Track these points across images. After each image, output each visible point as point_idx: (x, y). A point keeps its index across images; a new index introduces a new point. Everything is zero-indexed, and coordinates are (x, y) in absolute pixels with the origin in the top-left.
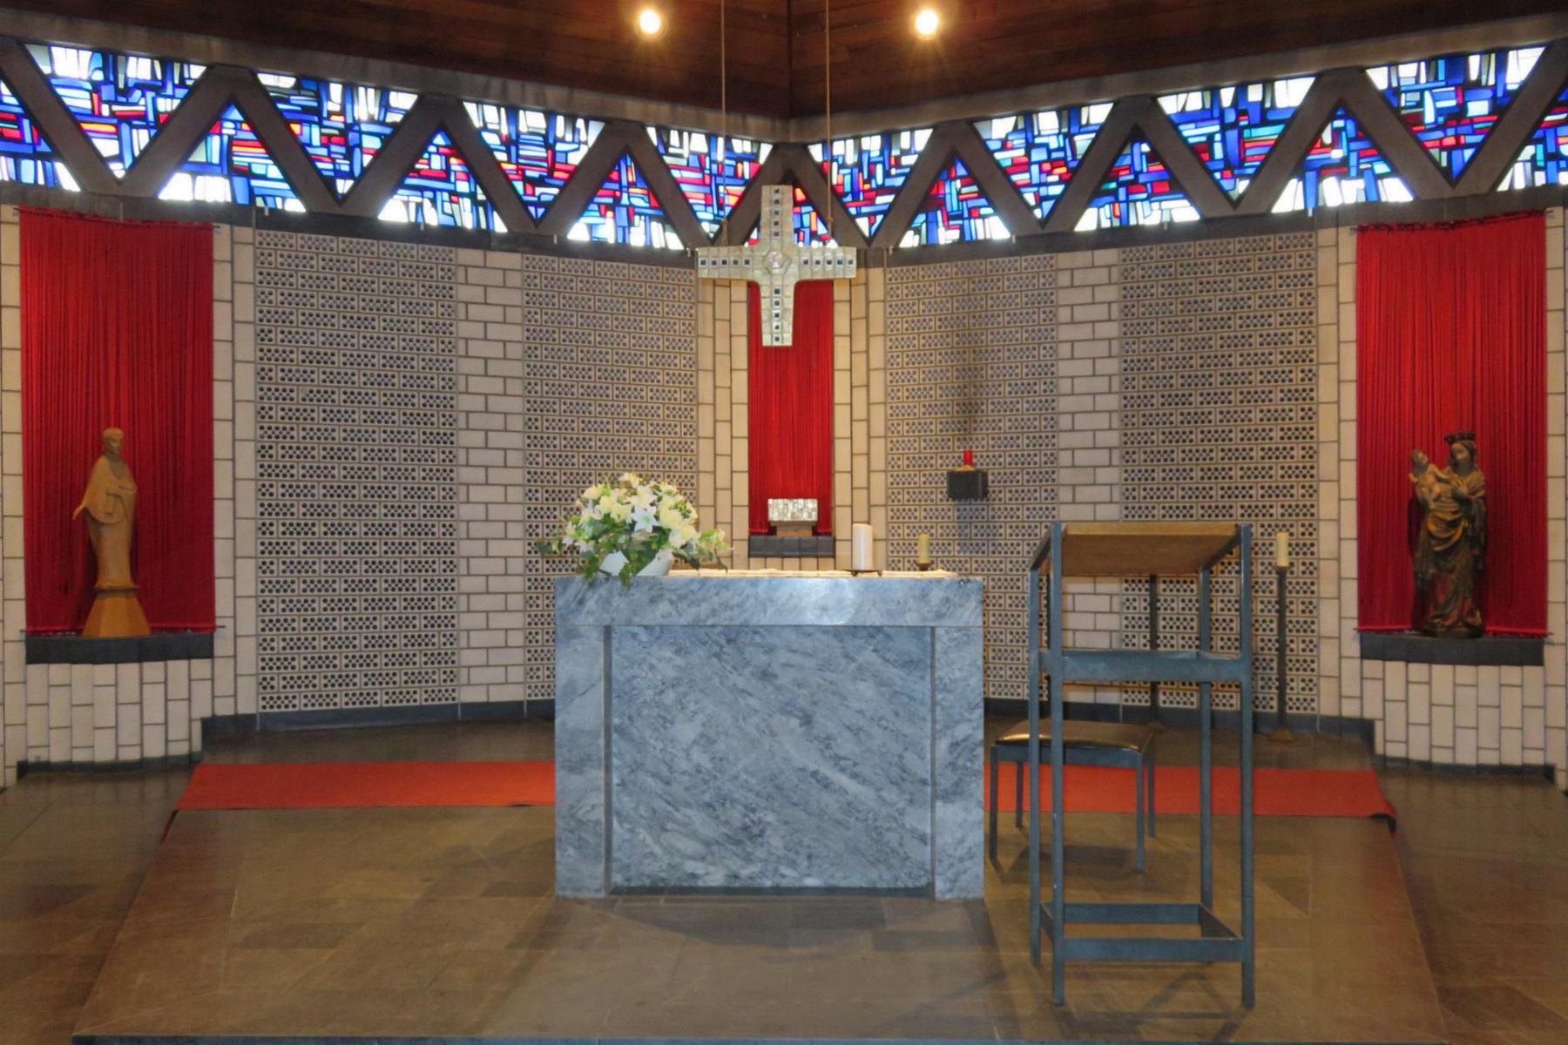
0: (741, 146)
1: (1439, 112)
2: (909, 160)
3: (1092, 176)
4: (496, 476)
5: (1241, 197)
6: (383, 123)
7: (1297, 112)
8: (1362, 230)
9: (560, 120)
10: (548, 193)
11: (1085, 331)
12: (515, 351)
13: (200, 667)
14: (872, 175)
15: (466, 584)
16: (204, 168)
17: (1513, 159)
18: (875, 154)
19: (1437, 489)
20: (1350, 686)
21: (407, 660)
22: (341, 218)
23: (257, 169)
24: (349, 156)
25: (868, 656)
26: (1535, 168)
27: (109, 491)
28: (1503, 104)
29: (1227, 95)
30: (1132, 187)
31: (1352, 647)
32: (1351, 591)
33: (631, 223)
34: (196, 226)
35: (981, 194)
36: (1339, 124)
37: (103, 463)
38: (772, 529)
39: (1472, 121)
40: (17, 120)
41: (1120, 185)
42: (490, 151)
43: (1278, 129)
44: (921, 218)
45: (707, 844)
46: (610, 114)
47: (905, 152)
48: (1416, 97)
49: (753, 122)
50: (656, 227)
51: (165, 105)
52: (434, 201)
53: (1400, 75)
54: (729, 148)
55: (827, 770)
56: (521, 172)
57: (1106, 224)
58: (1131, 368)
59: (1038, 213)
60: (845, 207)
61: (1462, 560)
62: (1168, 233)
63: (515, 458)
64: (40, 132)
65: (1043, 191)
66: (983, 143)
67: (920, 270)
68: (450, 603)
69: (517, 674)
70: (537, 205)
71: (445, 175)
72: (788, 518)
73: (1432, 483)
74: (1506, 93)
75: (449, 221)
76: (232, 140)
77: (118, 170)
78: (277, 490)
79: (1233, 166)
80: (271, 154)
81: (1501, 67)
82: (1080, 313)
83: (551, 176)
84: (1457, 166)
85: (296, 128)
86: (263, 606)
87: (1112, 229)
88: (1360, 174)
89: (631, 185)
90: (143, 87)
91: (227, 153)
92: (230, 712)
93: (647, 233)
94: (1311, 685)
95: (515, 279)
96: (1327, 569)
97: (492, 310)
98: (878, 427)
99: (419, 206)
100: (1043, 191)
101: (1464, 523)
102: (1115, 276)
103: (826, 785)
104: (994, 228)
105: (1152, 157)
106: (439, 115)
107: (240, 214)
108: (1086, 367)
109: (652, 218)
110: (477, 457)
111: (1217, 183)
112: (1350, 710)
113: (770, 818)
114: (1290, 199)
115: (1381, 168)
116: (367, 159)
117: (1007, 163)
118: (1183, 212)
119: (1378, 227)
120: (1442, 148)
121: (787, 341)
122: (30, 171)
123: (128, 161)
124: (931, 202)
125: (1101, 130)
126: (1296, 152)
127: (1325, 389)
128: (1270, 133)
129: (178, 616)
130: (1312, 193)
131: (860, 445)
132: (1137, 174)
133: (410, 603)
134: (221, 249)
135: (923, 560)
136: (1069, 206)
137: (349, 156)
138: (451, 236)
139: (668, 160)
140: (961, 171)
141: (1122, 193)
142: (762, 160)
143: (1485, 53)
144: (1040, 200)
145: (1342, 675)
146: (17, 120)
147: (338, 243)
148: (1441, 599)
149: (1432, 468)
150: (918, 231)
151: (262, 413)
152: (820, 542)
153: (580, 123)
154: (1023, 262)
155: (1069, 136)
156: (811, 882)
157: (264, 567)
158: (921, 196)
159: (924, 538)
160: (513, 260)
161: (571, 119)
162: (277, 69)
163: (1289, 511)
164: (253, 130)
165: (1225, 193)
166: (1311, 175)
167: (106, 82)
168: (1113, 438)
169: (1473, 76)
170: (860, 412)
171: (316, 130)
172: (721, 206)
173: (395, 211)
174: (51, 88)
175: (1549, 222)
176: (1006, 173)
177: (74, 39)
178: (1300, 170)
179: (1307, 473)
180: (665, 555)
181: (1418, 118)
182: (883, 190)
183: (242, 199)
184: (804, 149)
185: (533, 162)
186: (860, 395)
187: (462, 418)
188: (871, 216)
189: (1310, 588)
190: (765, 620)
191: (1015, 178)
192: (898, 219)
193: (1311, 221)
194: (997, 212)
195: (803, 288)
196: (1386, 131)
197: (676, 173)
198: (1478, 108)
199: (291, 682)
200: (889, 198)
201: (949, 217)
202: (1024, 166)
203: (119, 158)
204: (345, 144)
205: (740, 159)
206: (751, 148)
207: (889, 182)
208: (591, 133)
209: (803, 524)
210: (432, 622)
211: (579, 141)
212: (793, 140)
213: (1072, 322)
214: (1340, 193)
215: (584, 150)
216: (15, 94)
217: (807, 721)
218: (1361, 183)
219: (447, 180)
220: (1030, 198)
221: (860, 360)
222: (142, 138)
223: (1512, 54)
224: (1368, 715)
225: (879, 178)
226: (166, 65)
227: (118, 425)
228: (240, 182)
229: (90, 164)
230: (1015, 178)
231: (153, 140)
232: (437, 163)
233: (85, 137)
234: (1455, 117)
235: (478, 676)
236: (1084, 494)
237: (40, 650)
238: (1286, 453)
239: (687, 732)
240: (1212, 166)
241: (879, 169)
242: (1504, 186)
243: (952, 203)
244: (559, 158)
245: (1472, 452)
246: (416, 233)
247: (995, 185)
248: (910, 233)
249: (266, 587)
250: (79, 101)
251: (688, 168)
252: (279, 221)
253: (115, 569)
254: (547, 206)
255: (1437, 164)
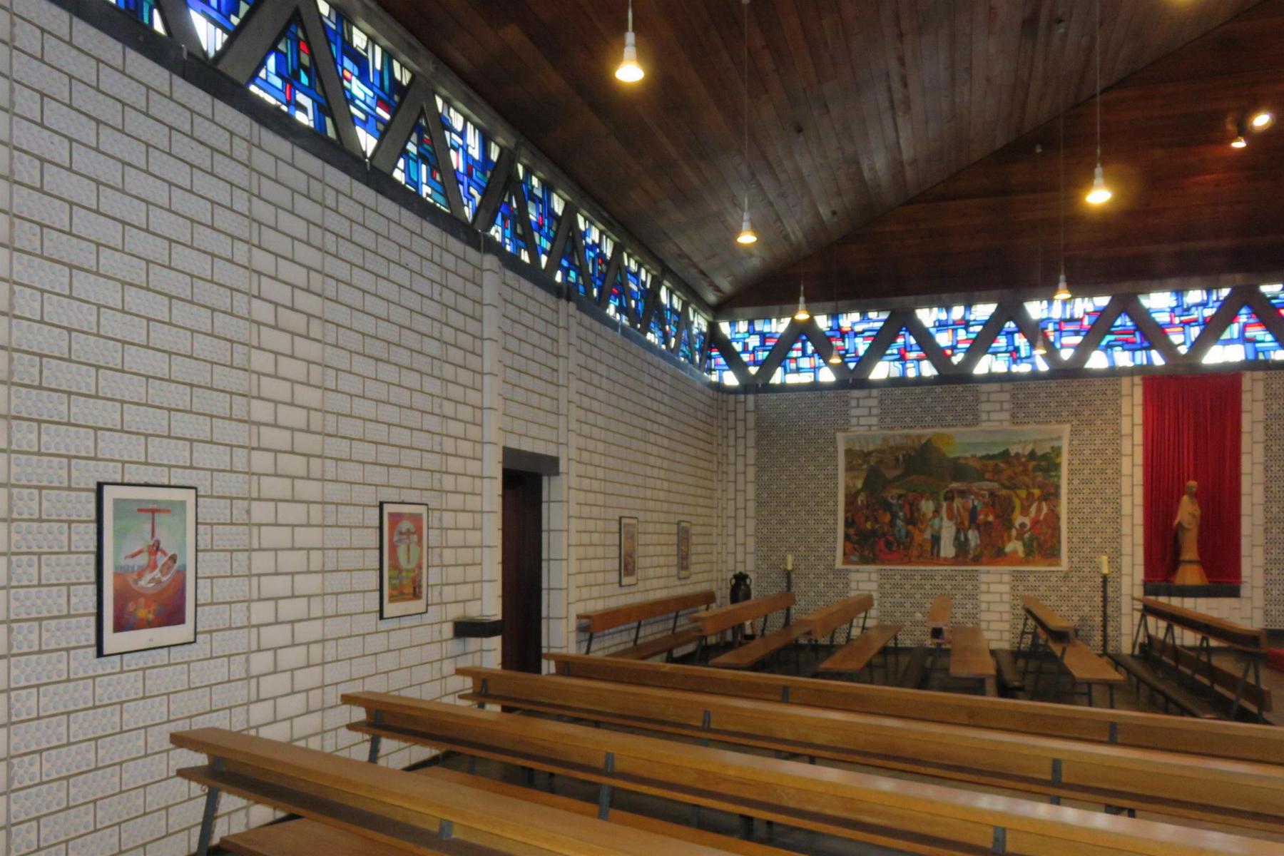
16: (1230, 341)
23: (1259, 338)
27: (1187, 512)
37: (1185, 498)
64: (1144, 336)
76: (1246, 325)
90: (1197, 305)
104: (730, 379)
122: (1141, 358)
123: (1188, 344)
129: (1223, 576)
183: (1251, 357)
203: (1184, 343)
222: (1195, 332)
226: (1209, 292)
227: (1195, 479)
228: (1249, 346)
229: (1169, 350)
231: (1202, 332)
237: (551, 465)
250: (1162, 318)
253: (1190, 551)
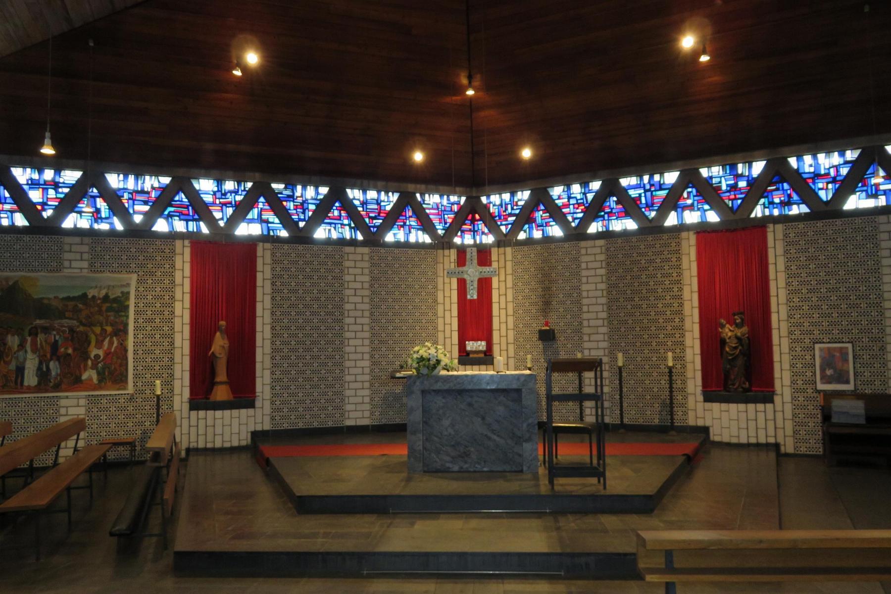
0: (454, 198)
1: (728, 185)
2: (521, 203)
3: (594, 210)
4: (359, 335)
5: (653, 218)
6: (316, 199)
7: (674, 186)
8: (698, 233)
9: (383, 193)
10: (378, 222)
11: (592, 272)
12: (366, 285)
13: (251, 411)
14: (506, 209)
15: (348, 378)
16: (252, 221)
17: (756, 204)
18: (508, 200)
19: (730, 334)
20: (700, 413)
21: (325, 408)
22: (301, 237)
23: (270, 220)
24: (304, 213)
25: (502, 398)
26: (765, 207)
27: (220, 344)
28: (752, 183)
29: (646, 178)
30: (610, 214)
31: (701, 398)
32: (699, 375)
33: (410, 232)
34: (251, 243)
35: (550, 217)
36: (690, 190)
38: (468, 354)
39: (740, 189)
40: (187, 207)
41: (606, 213)
42: (356, 207)
43: (666, 191)
44: (526, 226)
45: (453, 458)
46: (402, 190)
47: (519, 200)
48: (718, 180)
49: (458, 189)
50: (420, 233)
51: (239, 198)
52: (335, 228)
53: (713, 172)
54: (448, 199)
55: (490, 434)
56: (368, 214)
57: (600, 230)
58: (611, 287)
59: (573, 225)
60: (496, 222)
61: (740, 362)
62: (625, 234)
63: (366, 328)
64: (195, 211)
65: (575, 216)
66: (551, 197)
67: (526, 248)
68: (342, 386)
69: (367, 414)
70: (374, 227)
71: (339, 218)
72: (474, 349)
73: (728, 331)
74: (753, 179)
75: (341, 236)
77: (222, 224)
78: (278, 343)
79: (649, 206)
80: (276, 214)
81: (750, 167)
82: (590, 265)
83: (379, 215)
84: (735, 207)
85: (285, 203)
86: (272, 388)
87: (603, 232)
88: (699, 209)
89: (410, 217)
90: (231, 192)
91: (260, 215)
92: (260, 429)
93: (417, 235)
94: (685, 413)
95: (366, 258)
96: (689, 367)
97: (357, 272)
98: (510, 312)
99: (330, 230)
100: (575, 216)
101: (740, 347)
102: (603, 250)
103: (489, 438)
104: (556, 231)
105: (617, 203)
106: (337, 195)
107: (267, 238)
108: (593, 287)
109: (418, 229)
110: (352, 328)
111: (643, 213)
112: (700, 423)
113: (472, 449)
114: (672, 220)
115: (706, 207)
116: (310, 213)
117: (560, 204)
118: (630, 225)
119: (704, 232)
120: (730, 199)
121: (475, 297)
122: (192, 226)
123: (225, 220)
124: (530, 220)
125: (597, 193)
126: (673, 201)
127: (686, 294)
128: (663, 193)
130: (680, 217)
131: (503, 319)
132: (612, 209)
133: (327, 386)
134: (259, 252)
135: (529, 366)
136: (585, 222)
137: (304, 213)
138: (342, 242)
139: (424, 206)
140: (542, 207)
141: (606, 216)
142: (462, 203)
143: (744, 163)
144: (574, 219)
145: (699, 411)
146: (187, 207)
147: (301, 247)
148: (733, 377)
149: (728, 326)
150: (525, 231)
151: (273, 313)
152: (487, 358)
153: (390, 194)
154: (566, 245)
155: (585, 194)
156: (485, 469)
157: (272, 373)
158: (525, 217)
159: (529, 357)
160: (366, 250)
161: (387, 193)
162: (278, 181)
163: (675, 343)
164: (269, 205)
165: (647, 217)
166: (679, 210)
167: (218, 191)
168: (604, 315)
169: (740, 172)
170: (503, 305)
171: (292, 203)
172: (446, 223)
173: (320, 233)
174: (199, 194)
175: (768, 230)
176: (560, 208)
177: (207, 176)
178: (675, 208)
179: (681, 328)
180: (440, 367)
181: (719, 188)
182: (511, 215)
184: (478, 198)
185: (372, 211)
186: (503, 299)
187: (346, 312)
188: (506, 225)
189: (683, 374)
190: (470, 387)
191: (564, 210)
192: (517, 227)
193: (681, 228)
194: (557, 224)
195: (480, 281)
196: (709, 193)
197: (428, 211)
198: (742, 184)
199: (282, 418)
200: (514, 218)
201: (538, 226)
202: (567, 206)
203: (222, 219)
204: (303, 208)
205: (453, 204)
206: (458, 200)
207: (513, 212)
208: (394, 197)
209: (480, 352)
210: (335, 393)
211: (390, 200)
212: (474, 195)
213: (587, 269)
214: (691, 218)
215: (392, 204)
216: (187, 198)
217: (483, 418)
218: (699, 213)
219: (340, 219)
220: (570, 218)
221: (503, 284)
222: (230, 211)
223: (754, 164)
224: (707, 424)
225: (509, 210)
228: (264, 225)
229: (212, 222)
230: (564, 210)
231: (234, 211)
232: (336, 213)
233: (210, 212)
234: (734, 188)
235: (352, 415)
236: (593, 337)
238: (673, 320)
239: (446, 422)
240: (641, 206)
241: (509, 206)
242: (753, 215)
243: (539, 220)
244: (382, 208)
245: (742, 320)
246: (328, 242)
247: (556, 214)
248: (522, 232)
249: (274, 380)
250: (208, 199)
251: (432, 209)
252: (278, 240)
254: (377, 227)
255: (727, 206)
